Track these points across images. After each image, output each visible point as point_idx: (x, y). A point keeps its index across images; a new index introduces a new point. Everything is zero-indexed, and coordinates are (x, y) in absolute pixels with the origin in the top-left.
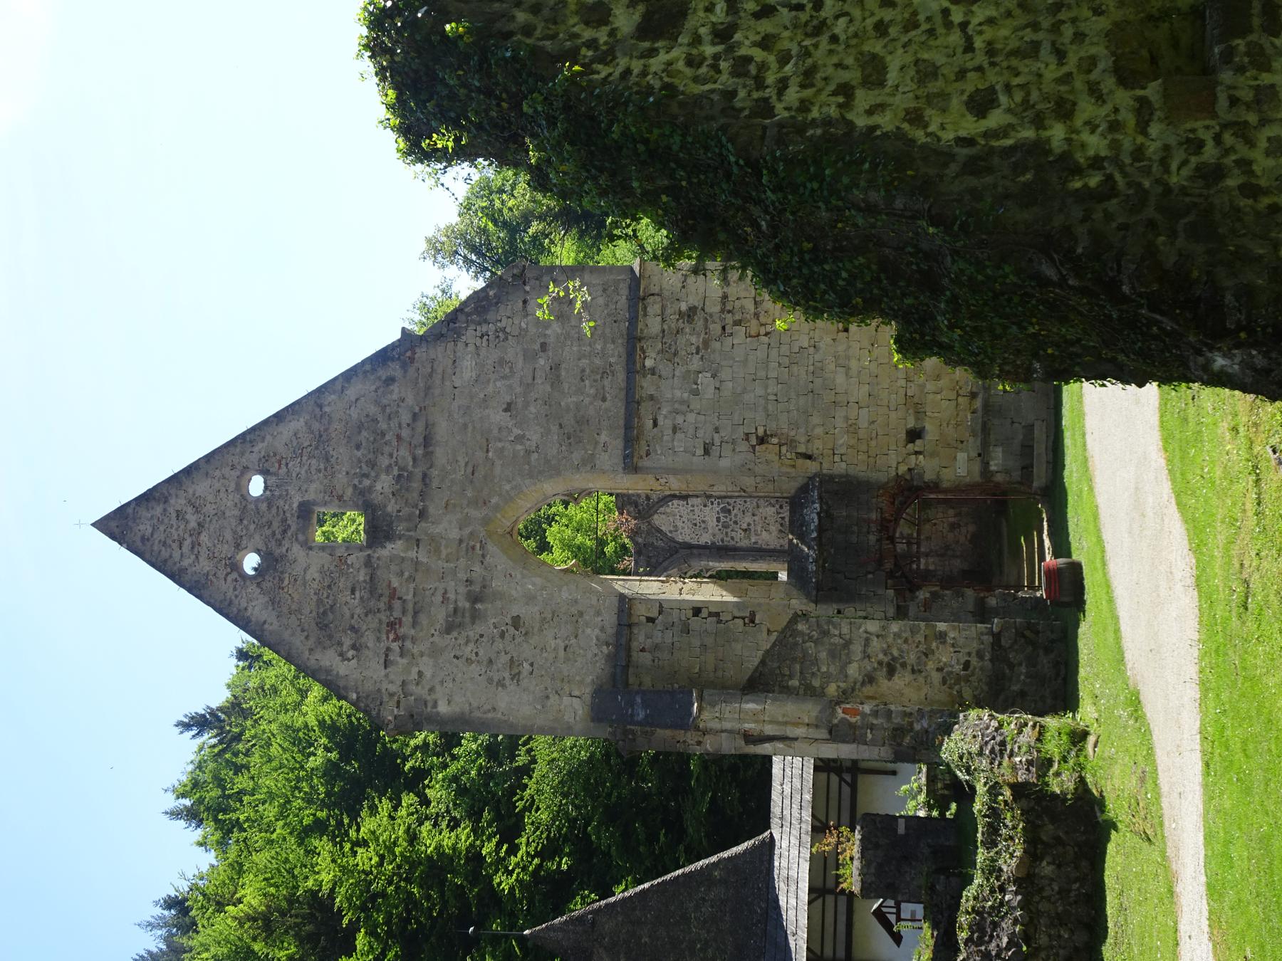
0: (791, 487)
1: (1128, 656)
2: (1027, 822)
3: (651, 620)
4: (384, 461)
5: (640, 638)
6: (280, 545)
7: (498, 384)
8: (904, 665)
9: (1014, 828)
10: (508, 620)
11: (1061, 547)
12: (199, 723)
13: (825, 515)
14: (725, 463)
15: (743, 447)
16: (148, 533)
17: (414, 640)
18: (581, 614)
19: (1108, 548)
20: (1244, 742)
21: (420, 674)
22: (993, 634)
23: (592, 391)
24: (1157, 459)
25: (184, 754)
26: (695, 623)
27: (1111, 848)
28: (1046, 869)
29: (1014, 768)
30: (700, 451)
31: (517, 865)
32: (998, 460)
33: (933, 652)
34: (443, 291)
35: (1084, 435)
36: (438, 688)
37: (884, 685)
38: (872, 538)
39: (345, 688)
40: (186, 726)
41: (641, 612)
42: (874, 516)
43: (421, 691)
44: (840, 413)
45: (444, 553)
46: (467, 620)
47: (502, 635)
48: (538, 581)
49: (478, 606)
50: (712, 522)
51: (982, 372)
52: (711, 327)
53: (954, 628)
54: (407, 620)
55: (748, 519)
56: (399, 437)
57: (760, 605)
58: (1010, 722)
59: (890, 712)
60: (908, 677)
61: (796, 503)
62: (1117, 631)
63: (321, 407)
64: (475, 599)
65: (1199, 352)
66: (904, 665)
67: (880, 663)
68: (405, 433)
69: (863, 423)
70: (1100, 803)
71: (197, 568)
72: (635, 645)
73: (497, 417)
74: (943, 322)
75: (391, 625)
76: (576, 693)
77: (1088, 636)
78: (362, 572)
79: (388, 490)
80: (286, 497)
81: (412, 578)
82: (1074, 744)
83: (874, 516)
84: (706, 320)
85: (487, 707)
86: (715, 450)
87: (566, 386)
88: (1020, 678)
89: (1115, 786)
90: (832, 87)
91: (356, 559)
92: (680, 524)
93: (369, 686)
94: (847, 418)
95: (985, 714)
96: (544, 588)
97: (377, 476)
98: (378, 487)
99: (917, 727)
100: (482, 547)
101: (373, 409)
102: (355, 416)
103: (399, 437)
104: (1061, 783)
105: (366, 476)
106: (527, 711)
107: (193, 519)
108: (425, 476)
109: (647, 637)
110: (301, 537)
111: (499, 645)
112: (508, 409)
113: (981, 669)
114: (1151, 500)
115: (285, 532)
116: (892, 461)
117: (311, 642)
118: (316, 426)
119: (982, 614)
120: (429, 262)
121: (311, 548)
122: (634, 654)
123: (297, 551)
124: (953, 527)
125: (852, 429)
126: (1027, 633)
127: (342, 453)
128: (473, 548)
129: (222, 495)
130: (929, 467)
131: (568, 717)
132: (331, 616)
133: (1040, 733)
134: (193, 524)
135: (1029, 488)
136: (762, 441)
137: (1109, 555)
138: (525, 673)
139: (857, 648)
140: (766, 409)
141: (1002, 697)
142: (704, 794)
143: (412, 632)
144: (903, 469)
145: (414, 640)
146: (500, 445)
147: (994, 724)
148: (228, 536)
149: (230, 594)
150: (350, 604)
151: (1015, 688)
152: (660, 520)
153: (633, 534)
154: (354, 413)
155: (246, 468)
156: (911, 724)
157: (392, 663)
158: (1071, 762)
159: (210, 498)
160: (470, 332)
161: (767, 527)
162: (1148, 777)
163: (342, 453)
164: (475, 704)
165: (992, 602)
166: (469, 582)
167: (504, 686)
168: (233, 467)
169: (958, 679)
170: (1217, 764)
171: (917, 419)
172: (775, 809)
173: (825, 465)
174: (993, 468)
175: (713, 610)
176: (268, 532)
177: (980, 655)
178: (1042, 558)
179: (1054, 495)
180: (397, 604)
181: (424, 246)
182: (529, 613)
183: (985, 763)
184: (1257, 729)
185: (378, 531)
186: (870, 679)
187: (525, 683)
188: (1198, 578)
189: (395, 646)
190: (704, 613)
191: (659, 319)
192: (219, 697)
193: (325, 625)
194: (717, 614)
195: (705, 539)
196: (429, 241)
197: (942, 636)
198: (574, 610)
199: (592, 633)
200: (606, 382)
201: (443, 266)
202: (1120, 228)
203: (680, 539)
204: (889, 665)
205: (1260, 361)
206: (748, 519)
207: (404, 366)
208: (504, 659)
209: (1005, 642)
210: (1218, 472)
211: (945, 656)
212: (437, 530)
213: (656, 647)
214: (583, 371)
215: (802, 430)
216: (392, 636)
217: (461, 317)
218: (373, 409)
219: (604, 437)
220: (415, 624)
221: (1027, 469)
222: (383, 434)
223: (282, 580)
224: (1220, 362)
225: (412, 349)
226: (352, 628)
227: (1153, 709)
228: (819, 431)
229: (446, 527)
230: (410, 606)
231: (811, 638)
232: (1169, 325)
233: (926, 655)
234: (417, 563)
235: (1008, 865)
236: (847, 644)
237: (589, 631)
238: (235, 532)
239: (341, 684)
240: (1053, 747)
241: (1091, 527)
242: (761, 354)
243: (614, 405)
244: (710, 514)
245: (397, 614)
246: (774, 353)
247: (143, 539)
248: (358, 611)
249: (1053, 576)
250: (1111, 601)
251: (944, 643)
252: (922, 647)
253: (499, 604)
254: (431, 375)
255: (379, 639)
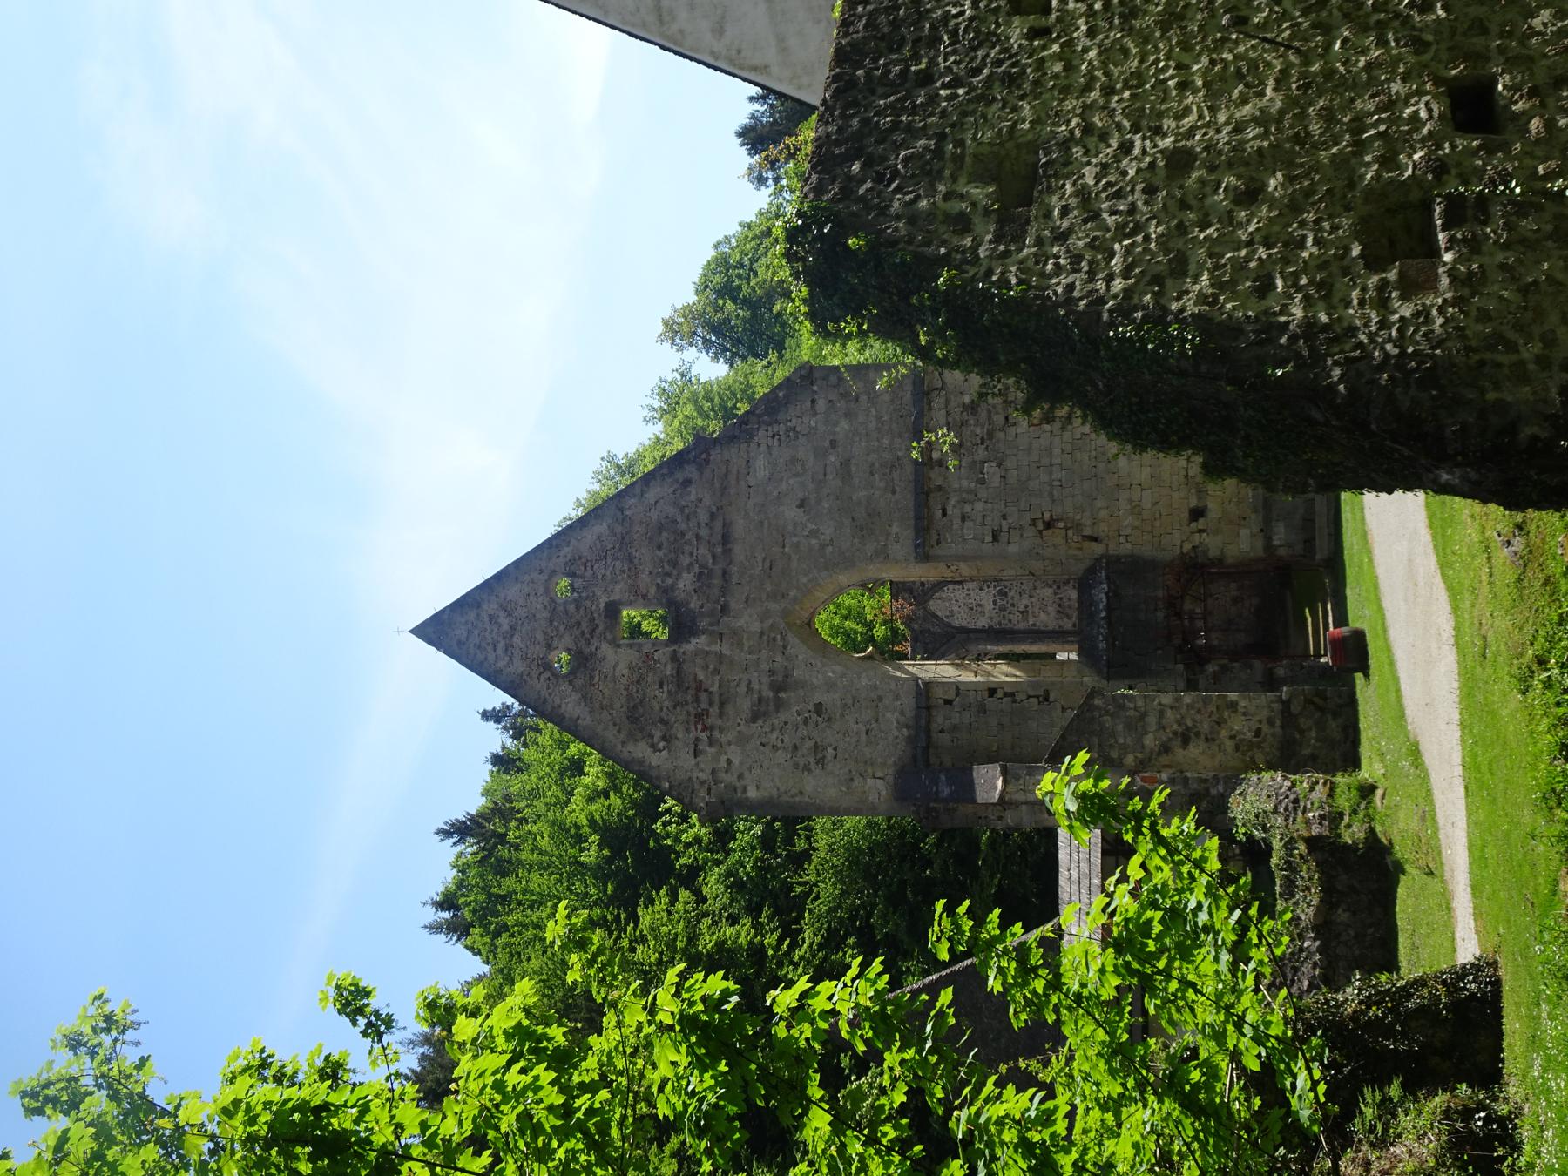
0: (1079, 569)
1: (1408, 712)
2: (1322, 873)
3: (948, 702)
4: (685, 561)
5: (939, 720)
6: (589, 643)
7: (791, 482)
8: (1198, 734)
9: (1310, 879)
10: (811, 707)
11: (1341, 620)
12: (459, 830)
13: (1114, 595)
14: (1013, 548)
15: (1030, 532)
16: (463, 638)
17: (721, 730)
18: (880, 699)
19: (1388, 615)
20: (1490, 764)
21: (729, 761)
22: (1283, 702)
23: (882, 485)
24: (1425, 535)
25: (440, 865)
26: (991, 703)
27: (1401, 892)
28: (1342, 915)
29: (1307, 822)
30: (989, 538)
31: (802, 958)
32: (1280, 535)
33: (1225, 721)
34: (682, 375)
35: (1362, 509)
36: (747, 774)
37: (1180, 754)
38: (1160, 615)
39: (658, 778)
40: (445, 833)
41: (939, 694)
42: (1160, 594)
43: (730, 778)
44: (1124, 496)
45: (747, 645)
46: (771, 708)
47: (806, 721)
48: (838, 668)
49: (782, 695)
50: (989, 606)
51: (1270, 488)
52: (995, 417)
53: (1244, 697)
54: (714, 711)
55: (1025, 601)
56: (698, 537)
57: (1053, 683)
58: (1303, 782)
59: (1186, 780)
60: (1202, 745)
61: (1085, 584)
62: (1398, 690)
63: (622, 510)
64: (778, 688)
65: (1429, 471)
66: (1198, 734)
67: (1175, 733)
68: (704, 532)
69: (1147, 504)
70: (1387, 850)
71: (512, 669)
72: (934, 726)
73: (791, 513)
74: (1240, 454)
75: (699, 717)
76: (879, 774)
77: (1367, 694)
78: (669, 667)
79: (690, 588)
80: (593, 598)
81: (717, 671)
82: (1363, 797)
83: (1160, 594)
84: (989, 412)
85: (794, 791)
86: (1003, 537)
87: (857, 481)
88: (1311, 742)
89: (1398, 829)
90: (1147, 279)
91: (662, 654)
92: (955, 609)
93: (680, 775)
94: (1130, 501)
95: (1279, 776)
96: (844, 675)
97: (679, 575)
98: (681, 585)
99: (1213, 792)
100: (783, 639)
101: (672, 511)
102: (654, 517)
103: (698, 537)
104: (1352, 833)
105: (669, 575)
106: (832, 793)
107: (505, 623)
108: (725, 573)
109: (946, 718)
110: (609, 636)
111: (803, 731)
112: (801, 506)
113: (1273, 735)
114: (1421, 570)
115: (593, 631)
116: (1177, 540)
117: (622, 736)
118: (619, 529)
119: (1271, 683)
120: (667, 345)
121: (619, 646)
122: (934, 735)
123: (606, 650)
124: (1235, 601)
125: (1136, 510)
126: (1316, 699)
127: (644, 554)
128: (774, 640)
129: (532, 598)
130: (1213, 544)
131: (873, 798)
132: (641, 710)
133: (1332, 789)
134: (505, 627)
135: (1314, 569)
136: (1049, 525)
137: (1389, 621)
138: (829, 757)
139: (1152, 720)
140: (1051, 495)
141: (1293, 762)
142: (992, 877)
143: (720, 722)
144: (1187, 547)
145: (721, 730)
146: (795, 540)
147: (1287, 783)
148: (540, 636)
149: (544, 692)
150: (659, 698)
151: (1306, 751)
152: (937, 606)
153: (908, 621)
154: (654, 515)
155: (554, 572)
156: (1207, 790)
157: (702, 752)
158: (1361, 815)
159: (521, 602)
160: (761, 433)
161: (1043, 607)
162: (1428, 816)
163: (644, 554)
164: (783, 789)
165: (1281, 672)
166: (772, 672)
167: (809, 771)
168: (541, 571)
169: (1251, 745)
170: (1473, 787)
171: (1199, 499)
172: (1063, 895)
173: (1111, 547)
174: (1276, 542)
175: (1008, 690)
176: (577, 632)
177: (1271, 722)
178: (1326, 627)
179: (1335, 565)
180: (703, 696)
181: (660, 328)
182: (829, 699)
183: (1280, 820)
184: (1497, 750)
185: (681, 625)
186: (1166, 749)
187: (829, 767)
188: (1456, 636)
189: (704, 736)
190: (1000, 694)
191: (943, 412)
192: (471, 802)
193: (636, 719)
194: (1012, 694)
195: (982, 622)
196: (666, 322)
197: (1233, 706)
198: (873, 695)
199: (892, 717)
200: (895, 475)
201: (681, 349)
202: (1367, 383)
203: (956, 623)
204: (1183, 734)
205: (1473, 475)
206: (1025, 601)
207: (700, 469)
208: (809, 744)
209: (1295, 709)
210: (1465, 551)
211: (1237, 724)
212: (740, 623)
213: (955, 728)
214: (873, 464)
215: (1087, 514)
216: (700, 727)
217: (753, 419)
218: (672, 511)
219: (895, 529)
220: (721, 715)
221: (1309, 542)
222: (683, 534)
223: (592, 677)
224: (1445, 477)
225: (707, 451)
226: (662, 721)
227: (1430, 758)
228: (1103, 513)
229: (747, 621)
230: (716, 698)
231: (1107, 712)
232: (1406, 452)
233: (1219, 724)
234: (720, 657)
235: (1307, 915)
236: (1143, 716)
237: (889, 715)
238: (546, 633)
239: (654, 773)
240: (1343, 802)
241: (1372, 596)
242: (1044, 442)
243: (905, 498)
244: (987, 598)
245: (704, 705)
246: (1057, 440)
247: (460, 643)
248: (667, 704)
249: (1338, 645)
250: (1392, 663)
251: (1236, 711)
252: (1214, 717)
253: (801, 692)
254: (726, 475)
255: (688, 730)
